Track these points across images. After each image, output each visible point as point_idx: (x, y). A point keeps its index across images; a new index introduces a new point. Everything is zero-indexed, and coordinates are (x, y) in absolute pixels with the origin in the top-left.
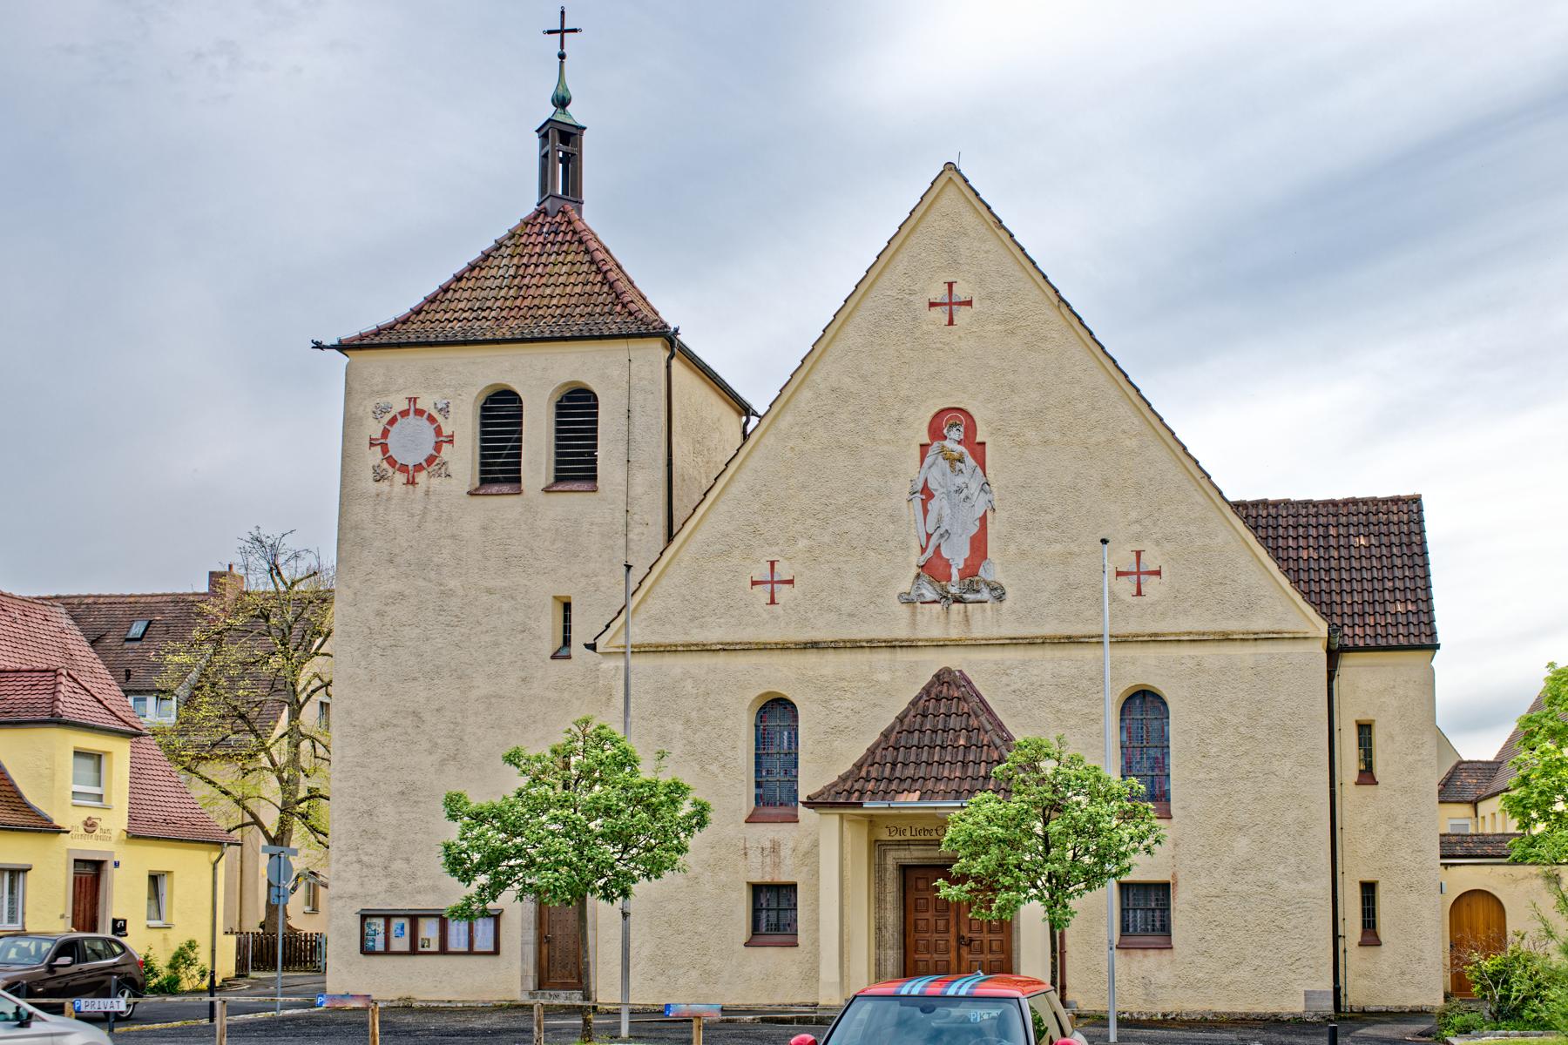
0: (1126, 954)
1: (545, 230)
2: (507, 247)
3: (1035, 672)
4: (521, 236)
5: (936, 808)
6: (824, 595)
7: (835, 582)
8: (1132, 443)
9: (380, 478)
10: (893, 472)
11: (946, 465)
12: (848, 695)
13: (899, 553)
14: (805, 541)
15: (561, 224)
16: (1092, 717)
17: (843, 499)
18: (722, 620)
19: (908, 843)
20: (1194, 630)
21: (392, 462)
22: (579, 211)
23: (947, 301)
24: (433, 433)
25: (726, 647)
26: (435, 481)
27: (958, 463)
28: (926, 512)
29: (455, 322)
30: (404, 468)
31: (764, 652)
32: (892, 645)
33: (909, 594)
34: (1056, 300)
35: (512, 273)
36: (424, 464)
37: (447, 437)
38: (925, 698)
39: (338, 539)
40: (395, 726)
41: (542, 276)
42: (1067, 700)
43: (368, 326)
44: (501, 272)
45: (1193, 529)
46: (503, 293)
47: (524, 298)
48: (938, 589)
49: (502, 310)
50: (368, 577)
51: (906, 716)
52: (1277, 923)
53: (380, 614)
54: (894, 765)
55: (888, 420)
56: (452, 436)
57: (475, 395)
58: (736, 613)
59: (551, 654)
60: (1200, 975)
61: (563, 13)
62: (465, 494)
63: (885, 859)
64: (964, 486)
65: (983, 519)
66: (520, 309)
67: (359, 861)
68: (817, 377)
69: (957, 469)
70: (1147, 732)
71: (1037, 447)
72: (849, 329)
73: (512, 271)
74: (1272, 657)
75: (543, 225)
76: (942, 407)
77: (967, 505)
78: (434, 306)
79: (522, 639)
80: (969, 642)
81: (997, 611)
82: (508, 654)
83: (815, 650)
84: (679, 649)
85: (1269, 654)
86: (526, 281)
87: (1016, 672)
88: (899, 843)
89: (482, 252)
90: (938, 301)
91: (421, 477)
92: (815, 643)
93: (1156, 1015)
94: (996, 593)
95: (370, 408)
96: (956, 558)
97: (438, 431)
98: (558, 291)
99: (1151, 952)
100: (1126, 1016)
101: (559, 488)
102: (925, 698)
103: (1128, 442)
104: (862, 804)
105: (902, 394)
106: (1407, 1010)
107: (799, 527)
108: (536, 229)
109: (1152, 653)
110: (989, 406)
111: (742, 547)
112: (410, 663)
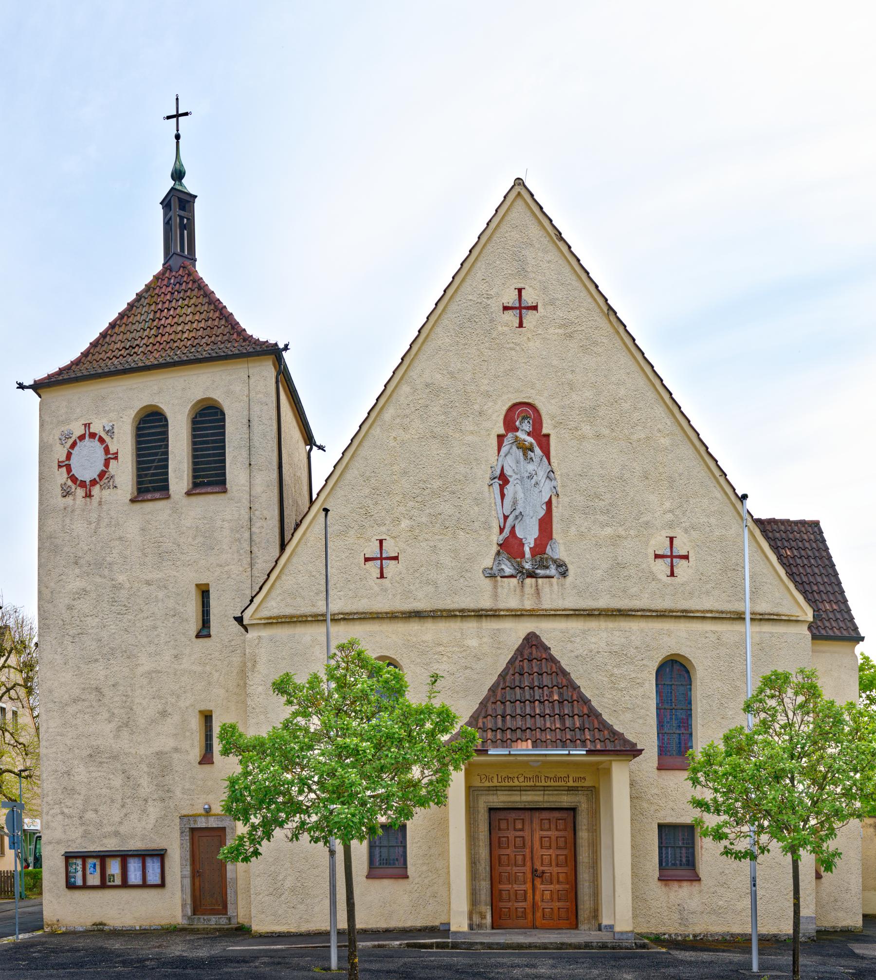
0: (666, 885)
1: (172, 281)
2: (145, 298)
3: (593, 640)
4: (154, 289)
5: (546, 755)
6: (423, 569)
7: (432, 558)
8: (665, 441)
9: (66, 494)
10: (476, 459)
11: (520, 453)
12: (445, 658)
13: (481, 532)
14: (408, 521)
15: (183, 277)
16: (638, 681)
17: (436, 484)
18: (340, 593)
19: (496, 789)
20: (715, 609)
21: (74, 479)
22: (194, 266)
23: (517, 305)
24: (103, 453)
25: (346, 617)
26: (106, 492)
27: (529, 452)
28: (503, 496)
29: (114, 359)
30: (83, 484)
31: (377, 621)
32: (480, 614)
33: (492, 569)
34: (605, 309)
35: (152, 317)
36: (97, 479)
37: (113, 454)
38: (520, 659)
39: (39, 548)
40: (83, 700)
41: (174, 317)
42: (618, 666)
43: (53, 368)
44: (143, 317)
45: (713, 520)
46: (146, 333)
47: (163, 335)
48: (515, 565)
49: (147, 346)
50: (60, 578)
51: (507, 674)
52: (777, 860)
53: (70, 608)
54: (504, 717)
55: (472, 413)
56: (117, 453)
57: (133, 416)
58: (352, 586)
59: (195, 634)
60: (721, 903)
61: (177, 99)
62: (128, 501)
63: (478, 802)
64: (534, 472)
65: (549, 504)
66: (161, 344)
67: (62, 813)
68: (413, 374)
69: (529, 457)
70: (675, 696)
71: (592, 441)
72: (439, 330)
73: (151, 316)
74: (772, 635)
75: (169, 279)
76: (515, 401)
77: (537, 490)
78: (98, 349)
79: (174, 622)
80: (541, 613)
81: (562, 585)
82: (163, 635)
83: (417, 619)
84: (309, 619)
85: (771, 633)
86: (162, 322)
87: (578, 640)
88: (489, 789)
89: (128, 304)
90: (510, 305)
91: (96, 490)
92: (418, 612)
93: (688, 936)
94: (562, 570)
95: (57, 435)
96: (529, 537)
97: (107, 450)
98: (187, 327)
99: (685, 884)
100: (666, 936)
101: (197, 491)
102: (520, 659)
103: (662, 440)
104: (487, 751)
105: (483, 388)
106: (839, 930)
107: (402, 509)
108: (165, 282)
109: (682, 628)
110: (553, 401)
111: (356, 527)
112: (92, 647)
